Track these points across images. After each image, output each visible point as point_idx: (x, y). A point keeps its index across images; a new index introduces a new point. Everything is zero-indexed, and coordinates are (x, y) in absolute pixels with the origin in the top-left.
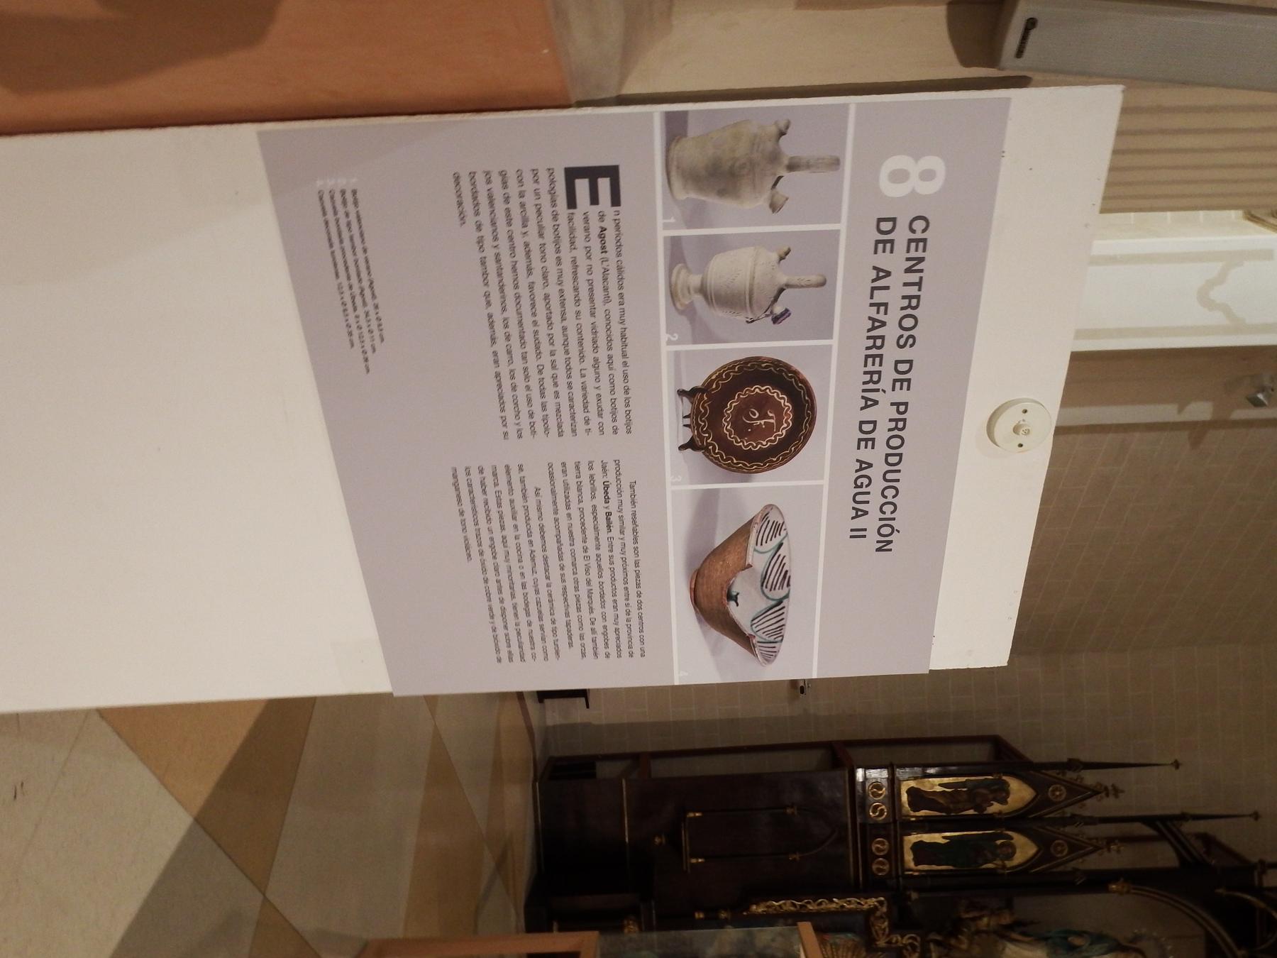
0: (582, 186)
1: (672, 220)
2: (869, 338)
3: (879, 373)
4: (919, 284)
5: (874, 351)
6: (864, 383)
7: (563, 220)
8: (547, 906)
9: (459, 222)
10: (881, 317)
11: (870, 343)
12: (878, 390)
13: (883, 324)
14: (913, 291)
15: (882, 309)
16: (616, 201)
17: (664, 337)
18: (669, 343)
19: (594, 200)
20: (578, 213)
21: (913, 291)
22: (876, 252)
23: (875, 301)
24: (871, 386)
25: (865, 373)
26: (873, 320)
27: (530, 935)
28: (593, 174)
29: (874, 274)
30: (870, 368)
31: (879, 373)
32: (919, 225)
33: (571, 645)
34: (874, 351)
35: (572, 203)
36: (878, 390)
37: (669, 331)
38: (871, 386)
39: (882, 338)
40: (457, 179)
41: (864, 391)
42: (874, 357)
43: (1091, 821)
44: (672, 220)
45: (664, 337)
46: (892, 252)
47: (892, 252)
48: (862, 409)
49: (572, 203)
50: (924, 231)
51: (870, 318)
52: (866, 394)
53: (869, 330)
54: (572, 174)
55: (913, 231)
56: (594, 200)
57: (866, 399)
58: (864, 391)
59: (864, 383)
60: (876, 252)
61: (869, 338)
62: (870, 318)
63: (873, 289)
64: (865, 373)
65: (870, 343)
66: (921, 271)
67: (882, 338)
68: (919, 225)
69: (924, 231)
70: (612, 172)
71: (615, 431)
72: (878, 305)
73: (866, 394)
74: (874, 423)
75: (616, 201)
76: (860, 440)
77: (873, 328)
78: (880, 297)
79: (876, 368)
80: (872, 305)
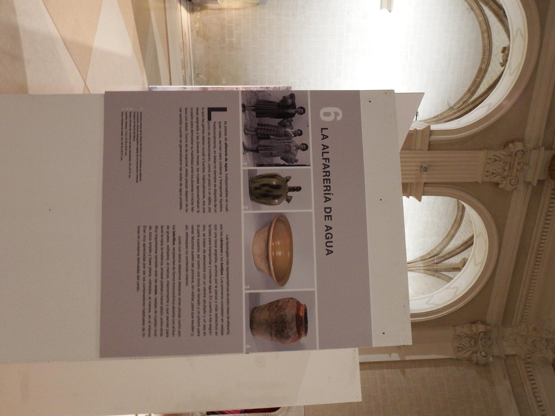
0: (327, 218)
2: (324, 172)
3: (330, 186)
5: (326, 177)
6: (325, 191)
10: (327, 163)
11: (325, 174)
12: (330, 194)
13: (329, 166)
15: (327, 160)
17: (243, 207)
18: (245, 210)
20: (211, 123)
23: (325, 157)
24: (327, 192)
25: (324, 186)
29: (322, 147)
30: (326, 184)
31: (330, 186)
33: (179, 237)
34: (326, 177)
36: (330, 194)
37: (245, 205)
38: (327, 192)
39: (329, 172)
41: (325, 194)
42: (327, 180)
45: (244, 287)
48: (327, 255)
50: (331, 238)
52: (326, 196)
57: (326, 198)
58: (325, 194)
59: (325, 191)
61: (324, 172)
63: (323, 153)
64: (324, 186)
65: (325, 174)
67: (329, 172)
72: (326, 159)
73: (326, 196)
74: (330, 208)
76: (326, 216)
77: (325, 168)
78: (326, 156)
79: (328, 184)
80: (323, 159)
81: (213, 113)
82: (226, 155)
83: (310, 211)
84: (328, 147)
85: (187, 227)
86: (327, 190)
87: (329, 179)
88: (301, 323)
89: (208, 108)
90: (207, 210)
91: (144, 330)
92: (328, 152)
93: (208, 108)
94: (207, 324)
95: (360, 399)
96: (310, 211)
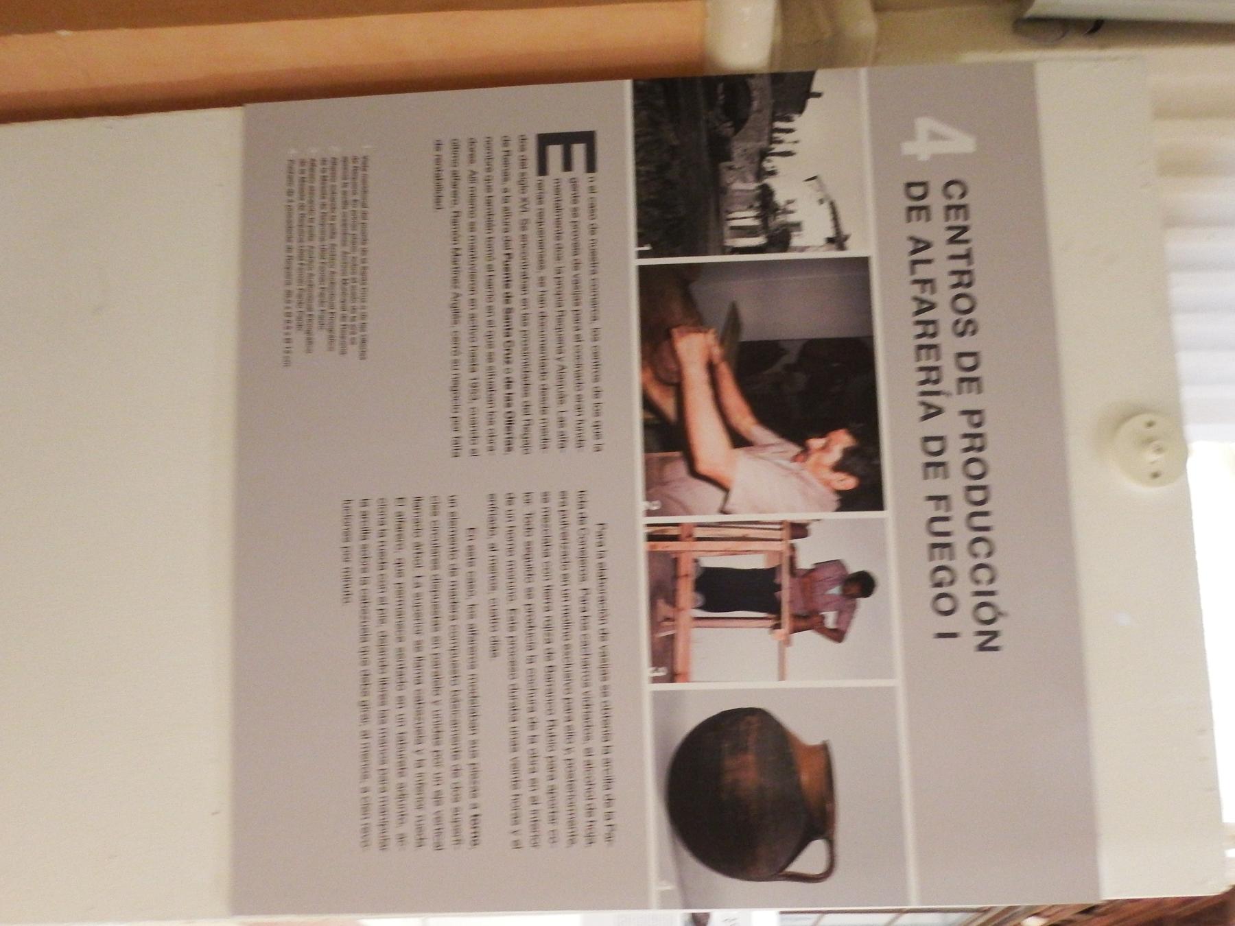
0: (555, 152)
1: (646, 248)
2: (918, 323)
4: (967, 256)
10: (927, 296)
12: (937, 393)
14: (961, 265)
16: (591, 166)
19: (568, 166)
20: (548, 181)
21: (961, 265)
23: (917, 277)
24: (928, 387)
26: (922, 301)
28: (566, 140)
31: (968, 272)
35: (543, 170)
36: (937, 393)
38: (928, 387)
44: (646, 248)
45: (643, 505)
49: (543, 170)
51: (916, 299)
54: (545, 141)
56: (568, 166)
57: (929, 406)
61: (918, 323)
62: (916, 299)
75: (591, 166)
78: (923, 272)
80: (916, 282)
81: (918, 266)
82: (596, 380)
84: (928, 246)
88: (811, 816)
89: (878, 505)
92: (928, 261)
93: (878, 505)
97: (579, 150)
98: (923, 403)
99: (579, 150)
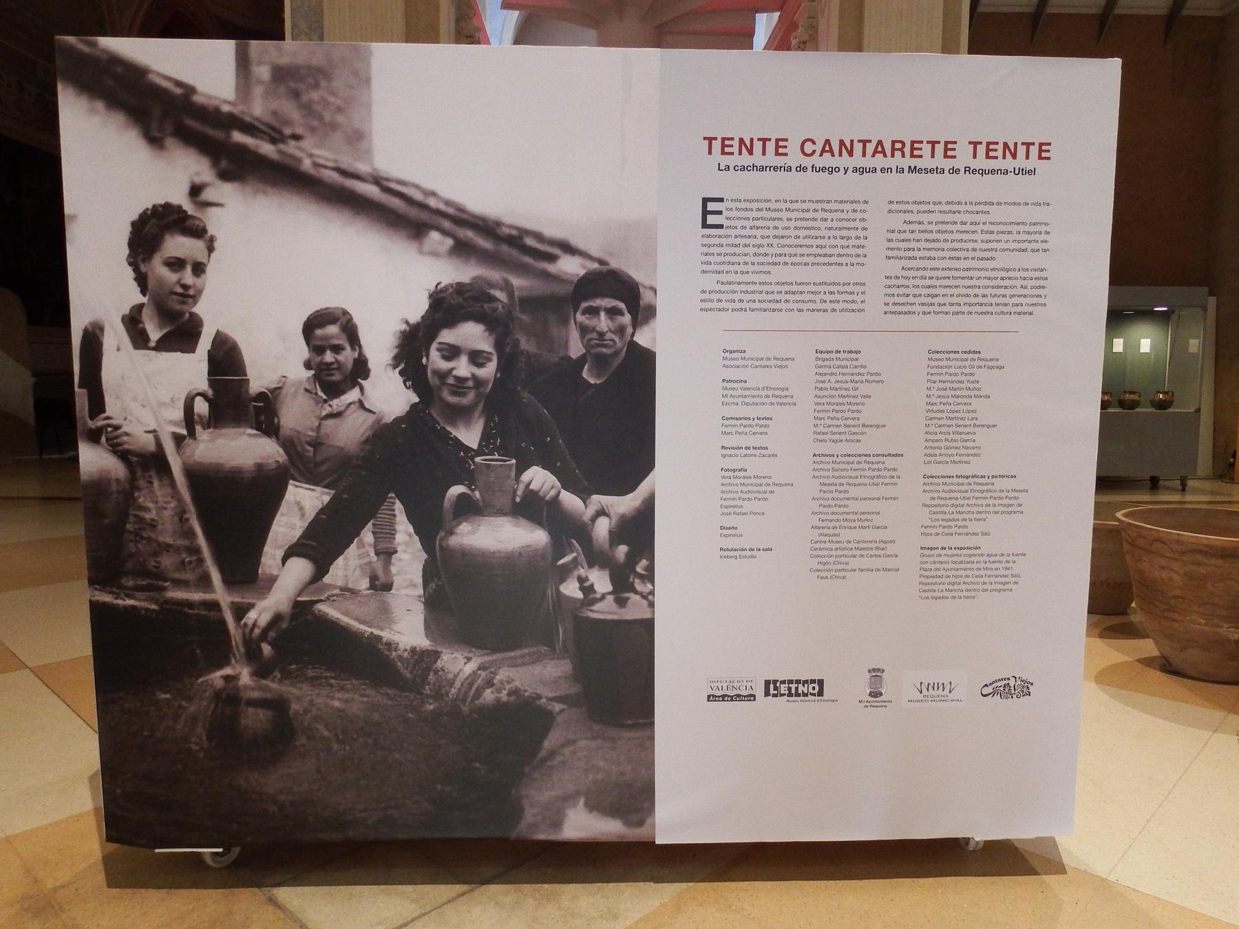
0: (916, 153)
2: (893, 156)
5: (907, 150)
6: (903, 156)
7: (729, 232)
8: (1232, 480)
9: (871, 667)
11: (898, 153)
13: (880, 143)
16: (721, 200)
19: (720, 213)
22: (1048, 158)
27: (115, 891)
28: (705, 213)
32: (809, 148)
34: (907, 150)
35: (721, 226)
39: (894, 142)
40: (704, 272)
42: (913, 149)
43: (1189, 503)
46: (1049, 144)
47: (1049, 144)
49: (721, 226)
50: (814, 143)
53: (885, 156)
54: (705, 225)
55: (814, 152)
56: (720, 213)
57: (875, 152)
59: (903, 156)
60: (1048, 158)
61: (893, 156)
65: (898, 153)
66: (852, 141)
67: (894, 142)
68: (809, 148)
69: (814, 143)
70: (705, 201)
71: (889, 241)
75: (721, 200)
83: (879, 223)
85: (866, 202)
86: (901, 150)
87: (913, 143)
90: (725, 392)
91: (769, 359)
94: (839, 242)
95: (1112, 68)
96: (879, 223)
97: (916, 145)
98: (873, 156)
99: (727, 142)
